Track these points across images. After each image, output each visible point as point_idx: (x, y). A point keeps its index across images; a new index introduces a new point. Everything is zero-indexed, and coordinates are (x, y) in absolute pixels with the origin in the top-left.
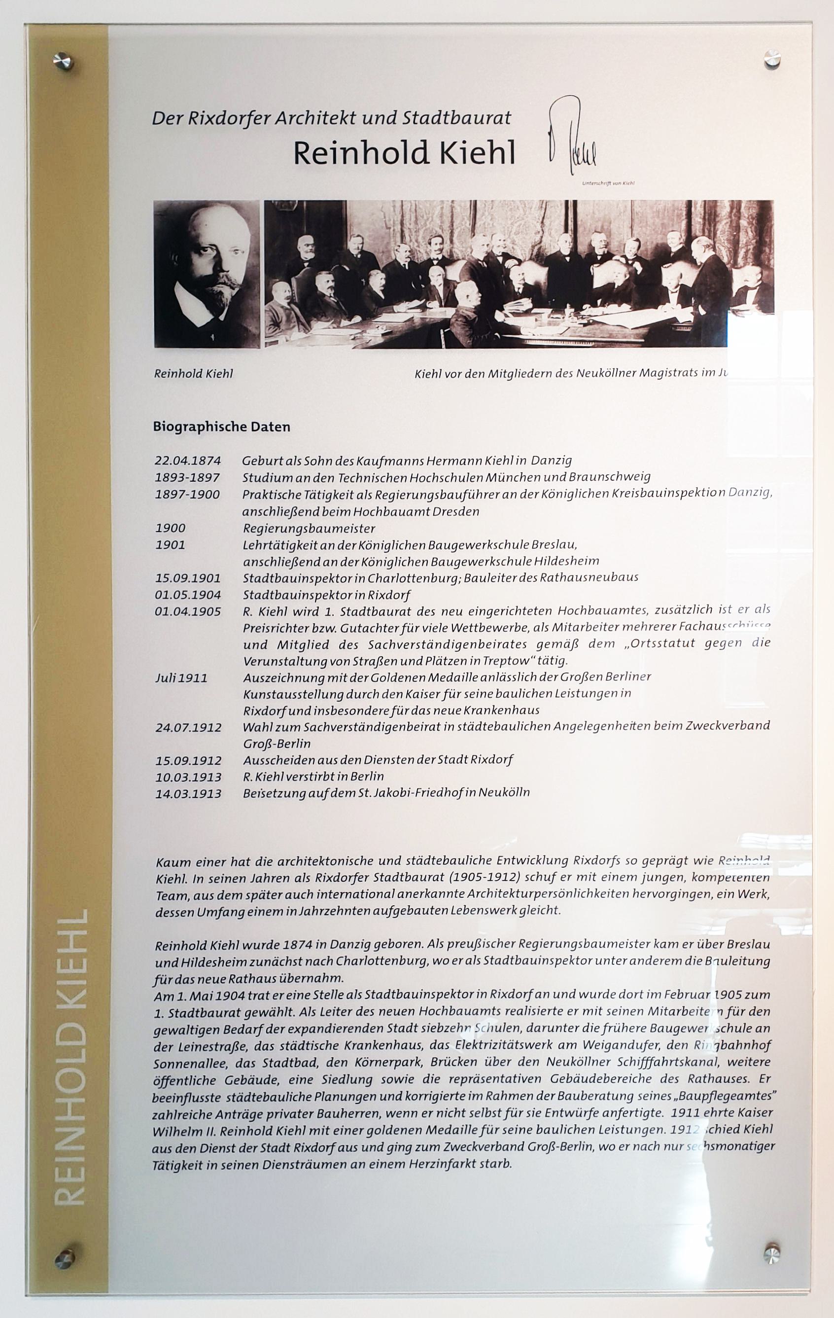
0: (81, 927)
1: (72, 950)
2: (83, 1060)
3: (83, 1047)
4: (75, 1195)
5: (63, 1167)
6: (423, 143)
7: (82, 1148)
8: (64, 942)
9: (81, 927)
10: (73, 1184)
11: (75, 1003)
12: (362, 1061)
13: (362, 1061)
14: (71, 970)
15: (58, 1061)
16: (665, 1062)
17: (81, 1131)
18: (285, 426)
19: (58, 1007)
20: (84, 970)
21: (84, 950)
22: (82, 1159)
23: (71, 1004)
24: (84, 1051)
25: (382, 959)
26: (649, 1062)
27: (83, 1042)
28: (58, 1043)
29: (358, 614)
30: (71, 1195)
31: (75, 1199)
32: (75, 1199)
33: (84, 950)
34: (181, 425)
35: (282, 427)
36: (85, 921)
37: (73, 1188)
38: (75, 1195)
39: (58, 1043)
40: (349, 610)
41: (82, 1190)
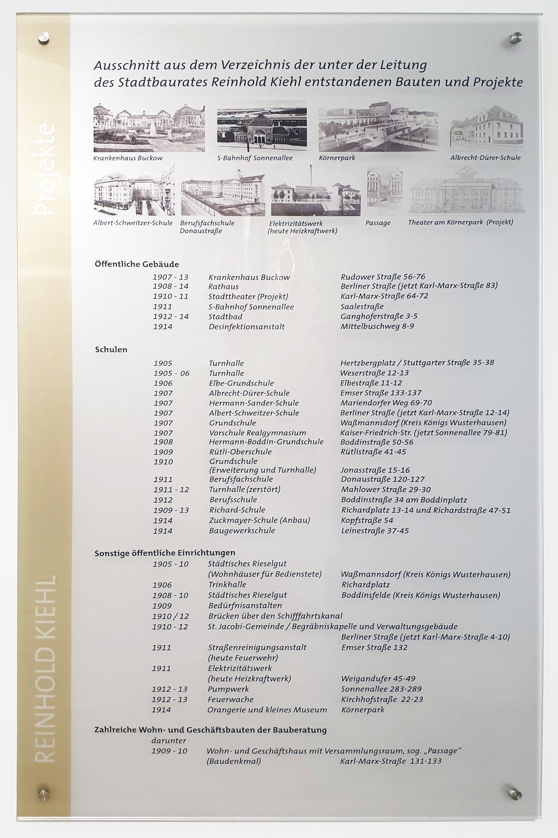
0: (52, 587)
1: (45, 601)
2: (53, 671)
3: (53, 663)
4: (49, 756)
5: (40, 738)
6: (265, 78)
7: (53, 726)
8: (40, 596)
9: (52, 587)
10: (48, 749)
11: (48, 635)
12: (323, 157)
13: (323, 157)
14: (45, 614)
15: (37, 671)
16: (309, 616)
17: (38, 725)
18: (232, 552)
19: (37, 637)
20: (53, 614)
21: (53, 602)
22: (53, 733)
23: (45, 636)
24: (54, 665)
25: (420, 362)
26: (298, 616)
27: (53, 660)
28: (37, 660)
29: (220, 318)
30: (46, 755)
31: (48, 759)
32: (48, 759)
33: (53, 602)
34: (290, 732)
35: (230, 553)
36: (54, 583)
37: (47, 751)
38: (49, 756)
39: (37, 660)
40: (214, 316)
41: (53, 753)
